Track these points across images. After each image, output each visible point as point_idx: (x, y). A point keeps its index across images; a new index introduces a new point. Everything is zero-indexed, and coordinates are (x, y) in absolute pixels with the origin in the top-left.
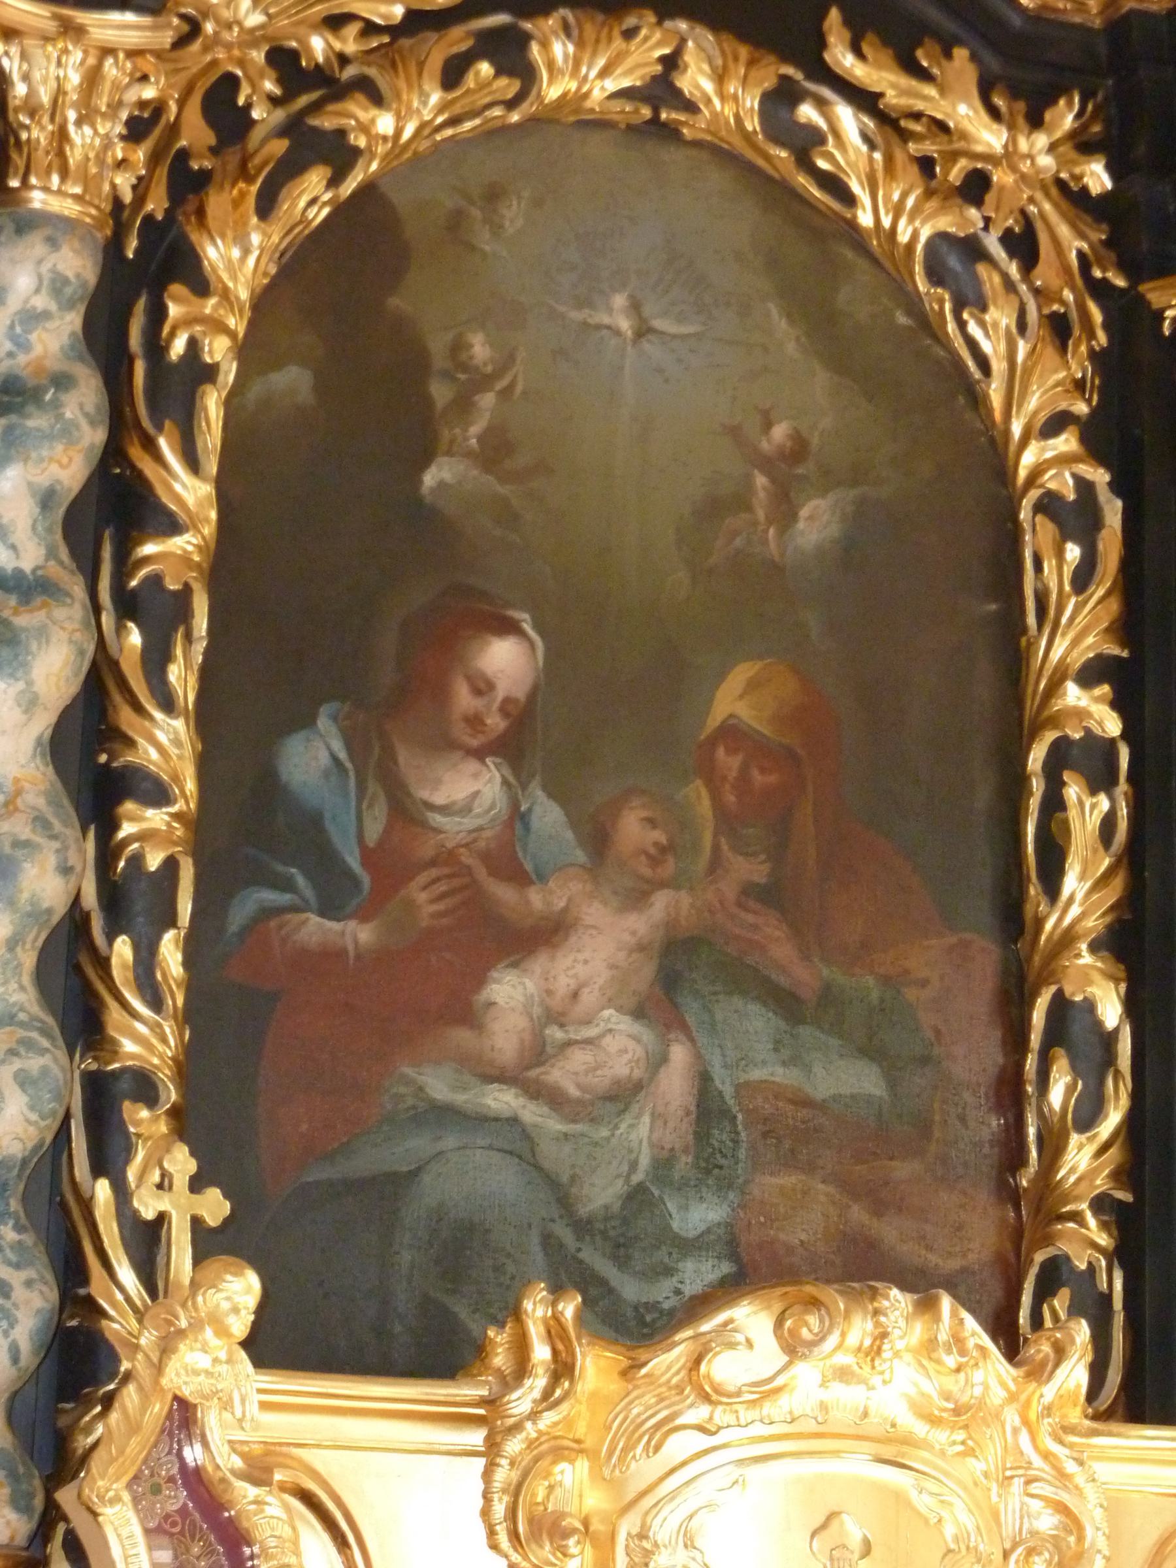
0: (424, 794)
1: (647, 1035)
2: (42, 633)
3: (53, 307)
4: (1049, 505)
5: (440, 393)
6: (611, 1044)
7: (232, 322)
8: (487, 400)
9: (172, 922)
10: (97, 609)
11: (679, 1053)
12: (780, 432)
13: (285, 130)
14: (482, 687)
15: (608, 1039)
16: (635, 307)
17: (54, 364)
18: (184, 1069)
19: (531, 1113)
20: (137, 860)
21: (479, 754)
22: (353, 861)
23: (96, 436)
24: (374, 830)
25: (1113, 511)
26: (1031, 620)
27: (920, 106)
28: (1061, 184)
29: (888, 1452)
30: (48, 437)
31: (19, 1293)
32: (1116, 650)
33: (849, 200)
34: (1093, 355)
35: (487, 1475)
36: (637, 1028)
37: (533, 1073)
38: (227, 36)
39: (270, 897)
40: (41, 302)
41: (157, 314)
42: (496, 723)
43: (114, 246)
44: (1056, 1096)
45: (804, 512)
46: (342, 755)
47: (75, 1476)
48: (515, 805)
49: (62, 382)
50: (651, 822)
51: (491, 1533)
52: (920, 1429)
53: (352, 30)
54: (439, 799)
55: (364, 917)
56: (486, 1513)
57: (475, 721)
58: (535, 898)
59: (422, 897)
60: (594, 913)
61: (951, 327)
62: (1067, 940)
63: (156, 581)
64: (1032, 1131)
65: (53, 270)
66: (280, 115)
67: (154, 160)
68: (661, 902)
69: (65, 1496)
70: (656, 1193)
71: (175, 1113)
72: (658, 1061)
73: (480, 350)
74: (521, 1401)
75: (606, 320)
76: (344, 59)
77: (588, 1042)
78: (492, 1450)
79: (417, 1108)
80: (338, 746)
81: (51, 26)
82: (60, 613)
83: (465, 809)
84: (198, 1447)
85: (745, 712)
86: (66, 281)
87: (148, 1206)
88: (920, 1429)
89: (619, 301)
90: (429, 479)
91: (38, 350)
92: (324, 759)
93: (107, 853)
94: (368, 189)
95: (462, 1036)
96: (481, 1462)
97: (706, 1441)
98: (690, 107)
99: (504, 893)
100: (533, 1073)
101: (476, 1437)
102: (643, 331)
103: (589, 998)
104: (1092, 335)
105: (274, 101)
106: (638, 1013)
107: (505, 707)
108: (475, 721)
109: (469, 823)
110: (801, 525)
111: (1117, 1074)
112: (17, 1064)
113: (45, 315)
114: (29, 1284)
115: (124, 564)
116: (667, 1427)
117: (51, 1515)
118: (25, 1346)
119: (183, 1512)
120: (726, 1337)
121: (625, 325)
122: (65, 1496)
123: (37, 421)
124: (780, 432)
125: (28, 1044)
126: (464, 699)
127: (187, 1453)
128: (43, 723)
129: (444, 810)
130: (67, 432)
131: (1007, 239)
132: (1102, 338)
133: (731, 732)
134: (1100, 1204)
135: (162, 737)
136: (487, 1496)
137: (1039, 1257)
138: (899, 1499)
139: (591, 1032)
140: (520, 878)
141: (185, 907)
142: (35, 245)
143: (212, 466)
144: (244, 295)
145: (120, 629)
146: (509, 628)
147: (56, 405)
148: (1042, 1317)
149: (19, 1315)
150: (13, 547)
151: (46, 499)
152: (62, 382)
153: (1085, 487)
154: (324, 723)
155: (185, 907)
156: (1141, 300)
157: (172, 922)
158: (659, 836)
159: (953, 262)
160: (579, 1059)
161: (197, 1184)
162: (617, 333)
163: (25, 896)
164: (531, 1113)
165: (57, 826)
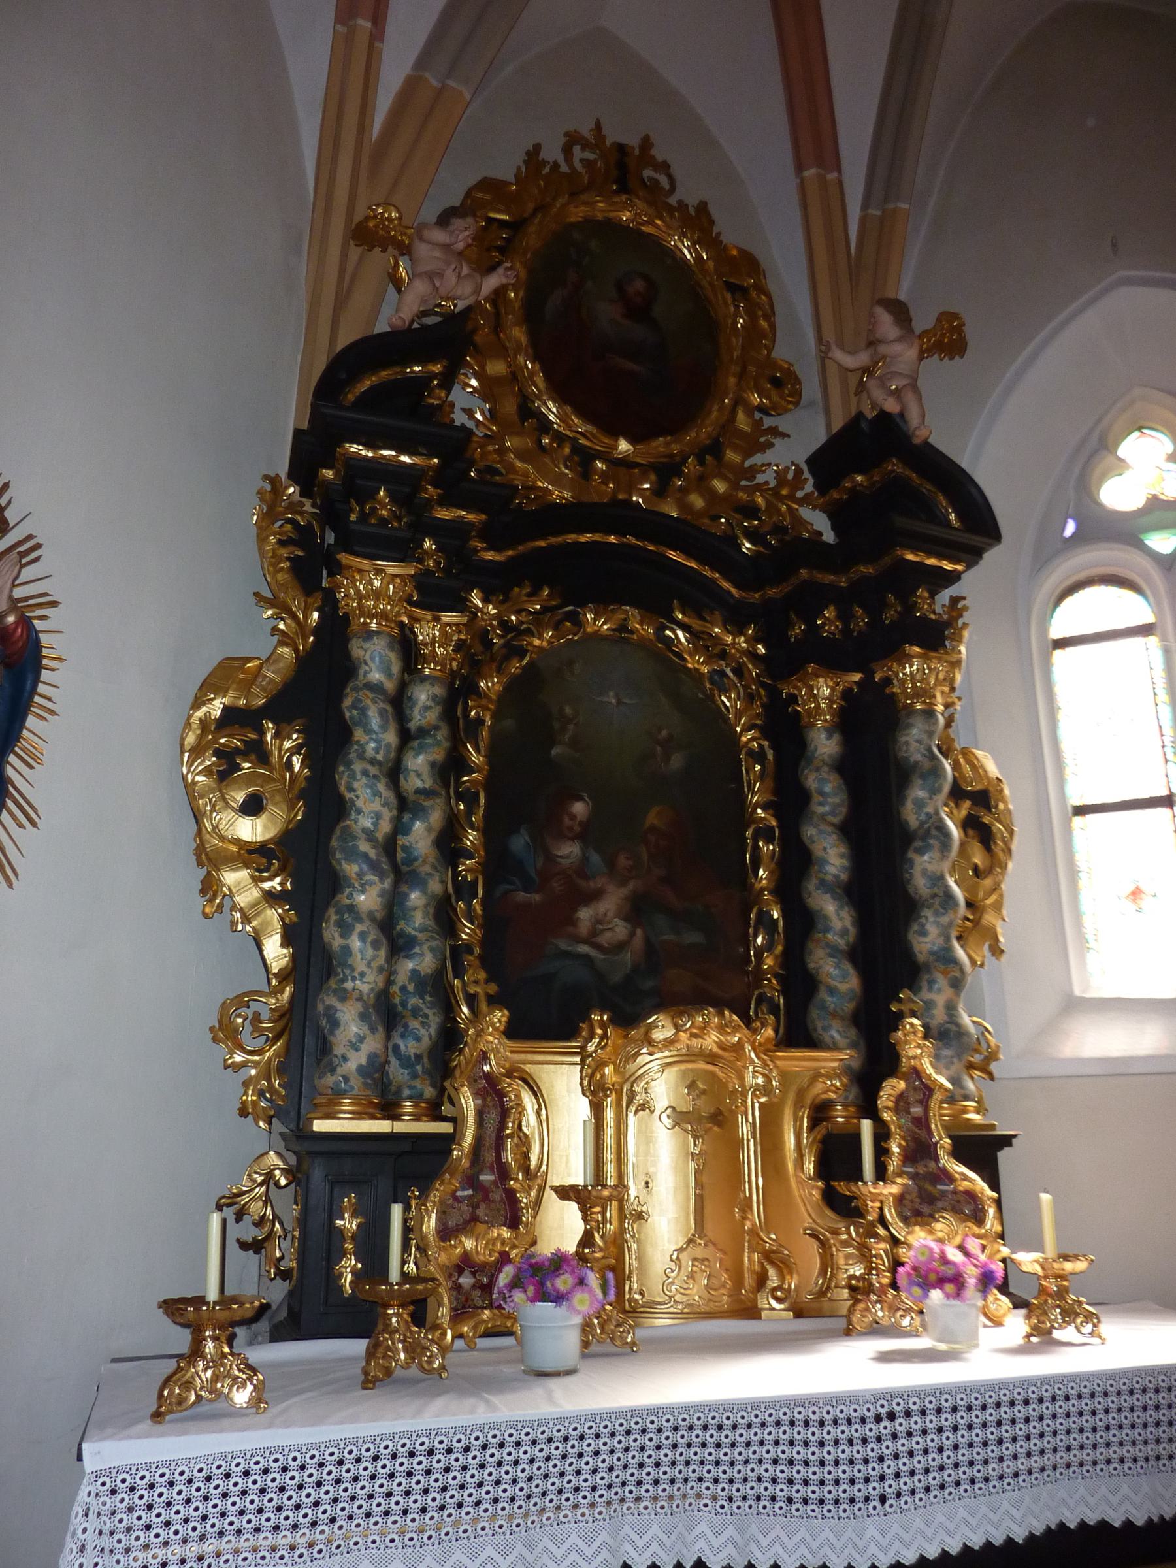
0: (555, 852)
1: (629, 926)
2: (432, 807)
3: (433, 705)
4: (751, 753)
5: (556, 725)
6: (618, 929)
7: (490, 706)
8: (571, 727)
9: (476, 897)
10: (450, 798)
11: (639, 931)
12: (664, 733)
13: (505, 646)
14: (573, 817)
15: (616, 928)
16: (617, 695)
17: (434, 722)
18: (483, 943)
19: (593, 953)
20: (465, 877)
21: (572, 839)
22: (533, 874)
23: (446, 745)
24: (540, 864)
25: (770, 755)
26: (746, 790)
27: (705, 630)
28: (750, 652)
29: (709, 1060)
30: (431, 745)
31: (431, 1017)
32: (772, 798)
33: (684, 659)
34: (762, 705)
35: (581, 1071)
36: (625, 924)
37: (593, 940)
38: (485, 617)
39: (508, 887)
40: (429, 703)
41: (466, 705)
42: (577, 829)
43: (452, 684)
44: (759, 940)
45: (673, 757)
46: (529, 841)
47: (37, 647)
48: (584, 855)
49: (436, 728)
50: (628, 859)
51: (583, 1090)
52: (720, 1052)
53: (524, 614)
54: (560, 853)
55: (537, 892)
56: (581, 1084)
57: (570, 828)
58: (592, 884)
59: (555, 885)
60: (611, 888)
61: (717, 698)
62: (762, 890)
63: (468, 789)
64: (752, 952)
65: (433, 693)
66: (502, 641)
67: (463, 657)
68: (631, 885)
69: (447, 1084)
70: (729, 639)
71: (480, 957)
72: (632, 934)
73: (568, 711)
74: (591, 1047)
75: (607, 700)
76: (523, 623)
77: (610, 929)
78: (582, 1062)
79: (527, 477)
80: (527, 838)
81: (430, 618)
82: (438, 801)
83: (568, 857)
84: (488, 1066)
85: (656, 822)
86: (437, 696)
87: (472, 990)
88: (720, 1052)
89: (611, 694)
90: (553, 752)
91: (428, 718)
92: (523, 842)
93: (456, 874)
94: (531, 663)
95: (570, 929)
96: (579, 1067)
97: (650, 1058)
98: (632, 632)
99: (582, 883)
100: (593, 940)
101: (577, 1059)
102: (619, 702)
103: (610, 914)
104: (761, 698)
105: (501, 637)
106: (626, 919)
107: (581, 823)
108: (570, 828)
109: (569, 861)
110: (672, 762)
111: (778, 933)
112: (429, 944)
113: (431, 707)
114: (434, 1014)
115: (458, 783)
116: (638, 1054)
117: (442, 1090)
118: (433, 1034)
119: (484, 1087)
120: (654, 1025)
121: (613, 701)
122: (447, 1084)
123: (429, 741)
124: (664, 733)
125: (432, 937)
126: (567, 821)
127: (485, 1068)
128: (433, 835)
129: (561, 857)
130: (438, 744)
131: (734, 671)
132: (765, 699)
133: (653, 829)
134: (776, 975)
135: (471, 838)
136: (581, 1078)
137: (756, 993)
138: (713, 1074)
139: (610, 926)
140: (586, 877)
141: (480, 892)
142: (427, 686)
143: (483, 752)
144: (494, 697)
145: (458, 805)
146: (581, 799)
147: (435, 735)
148: (1040, 734)
149: (432, 1024)
150: (422, 780)
151: (433, 765)
152: (436, 728)
153: (761, 746)
154: (522, 831)
155: (480, 892)
156: (776, 686)
157: (476, 897)
158: (631, 863)
159: (716, 677)
160: (608, 935)
161: (487, 981)
162: (611, 703)
163: (429, 891)
164: (593, 953)
165: (439, 867)
